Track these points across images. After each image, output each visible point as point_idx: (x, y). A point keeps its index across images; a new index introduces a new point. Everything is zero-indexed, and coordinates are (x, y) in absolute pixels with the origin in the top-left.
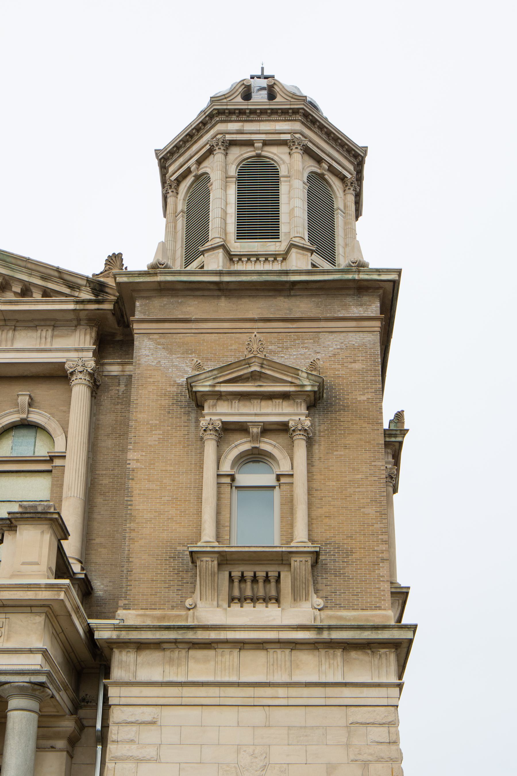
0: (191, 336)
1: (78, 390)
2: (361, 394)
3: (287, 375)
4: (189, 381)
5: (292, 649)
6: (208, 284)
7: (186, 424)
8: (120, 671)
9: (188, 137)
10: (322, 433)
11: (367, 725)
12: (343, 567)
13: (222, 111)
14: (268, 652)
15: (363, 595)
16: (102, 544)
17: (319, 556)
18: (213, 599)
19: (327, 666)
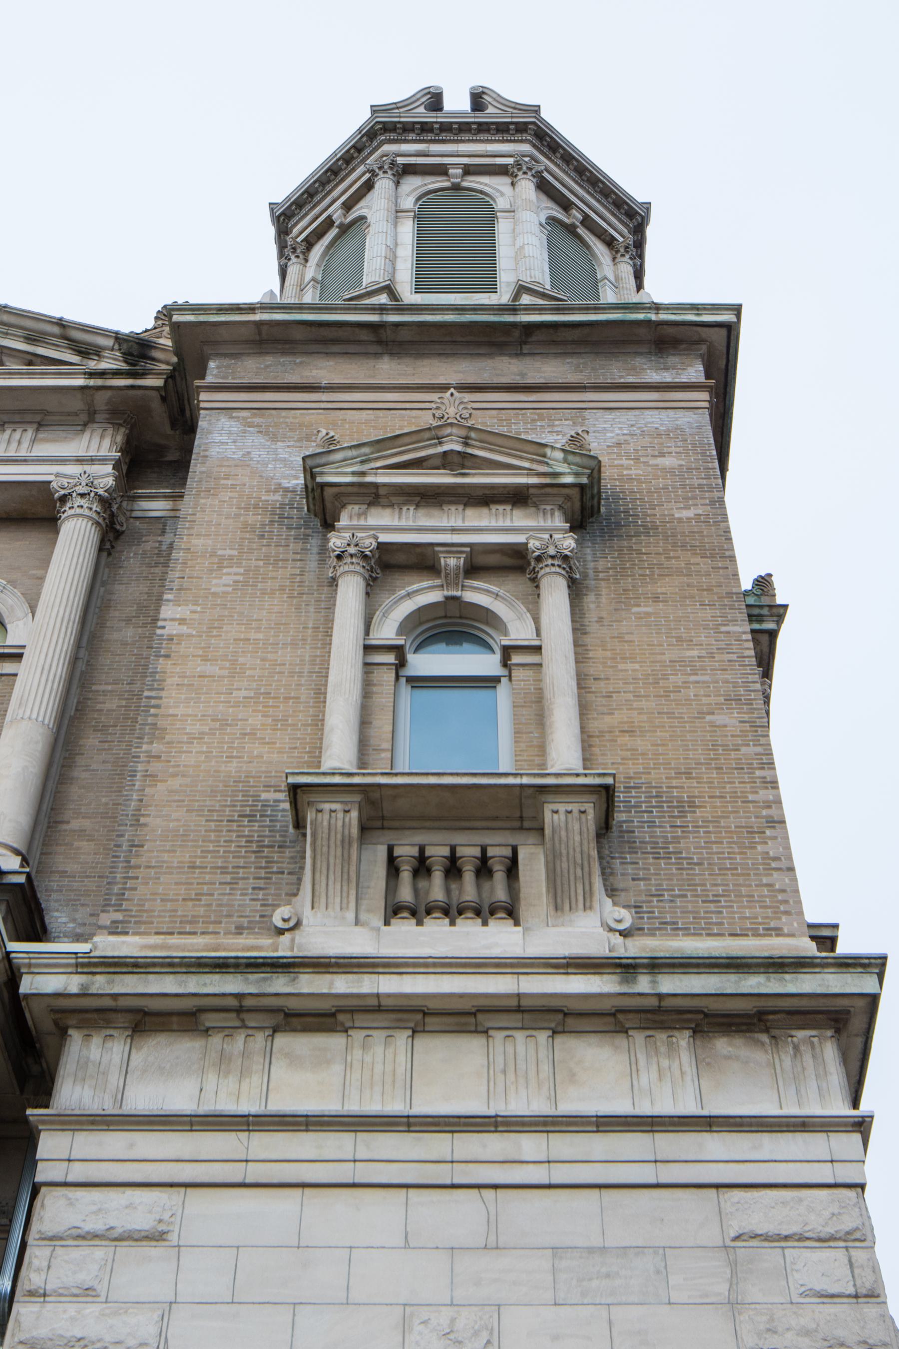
0: (318, 414)
1: (72, 526)
2: (681, 508)
3: (521, 458)
4: (310, 462)
5: (554, 1032)
6: (357, 330)
7: (298, 557)
8: (78, 1089)
9: (329, 174)
10: (601, 575)
11: (783, 1244)
12: (673, 837)
14: (491, 1040)
15: (731, 901)
16: (85, 831)
17: (613, 796)
18: (344, 906)
19: (654, 1075)
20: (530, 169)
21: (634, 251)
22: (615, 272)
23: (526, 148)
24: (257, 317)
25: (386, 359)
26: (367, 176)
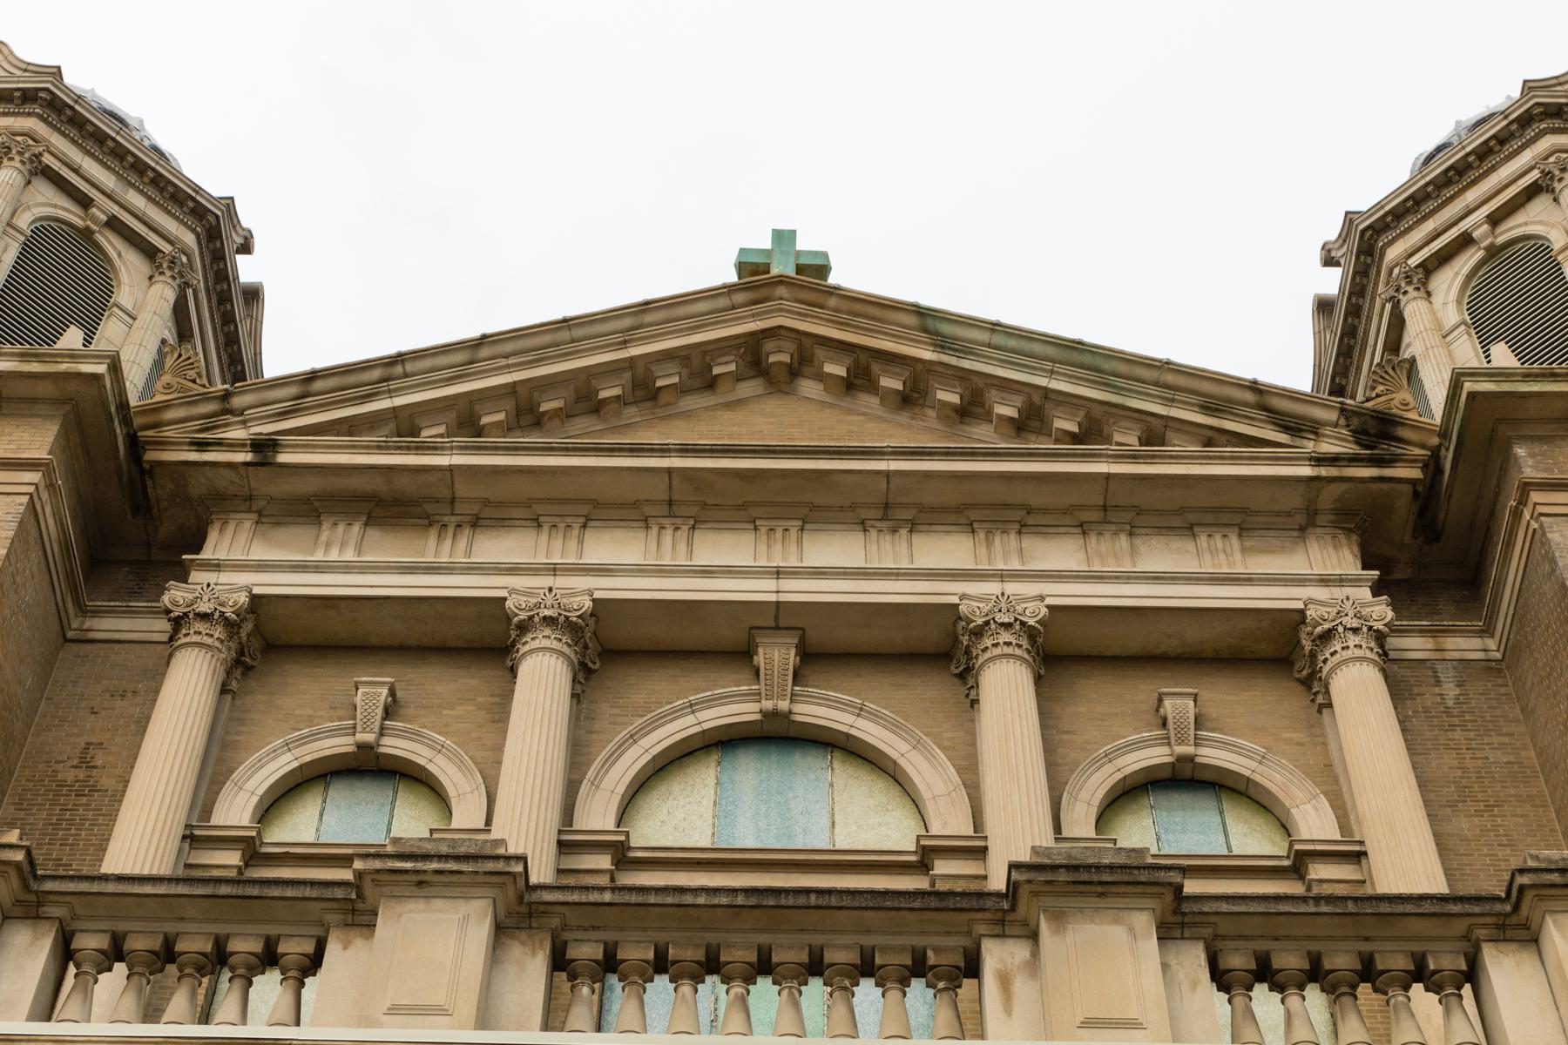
13: (1552, 110)
23: (189, 239)
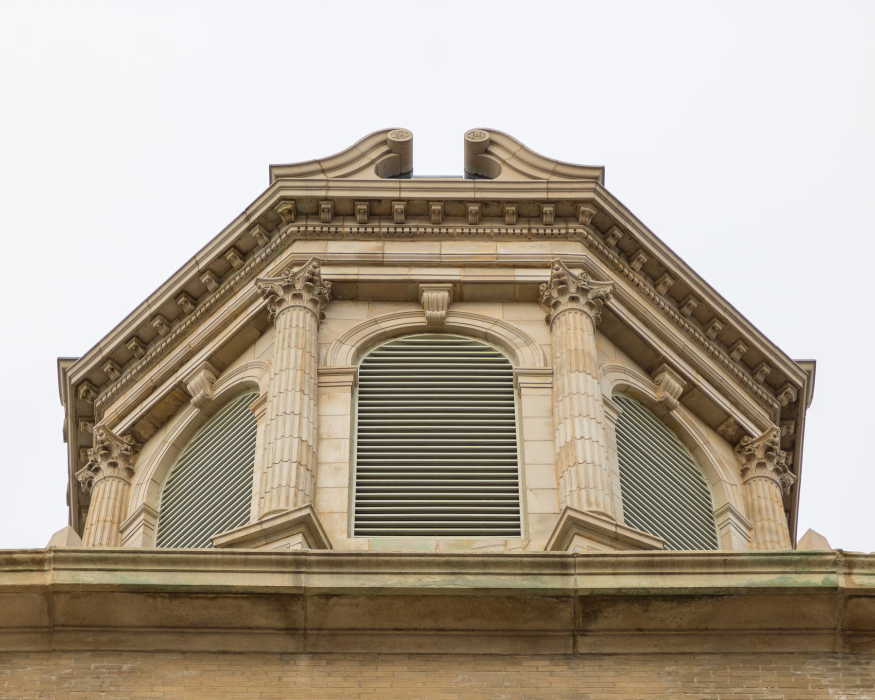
6: (246, 605)
9: (182, 300)
20: (584, 291)
21: (783, 457)
22: (745, 498)
23: (575, 250)
24: (49, 578)
25: (303, 663)
26: (261, 303)
